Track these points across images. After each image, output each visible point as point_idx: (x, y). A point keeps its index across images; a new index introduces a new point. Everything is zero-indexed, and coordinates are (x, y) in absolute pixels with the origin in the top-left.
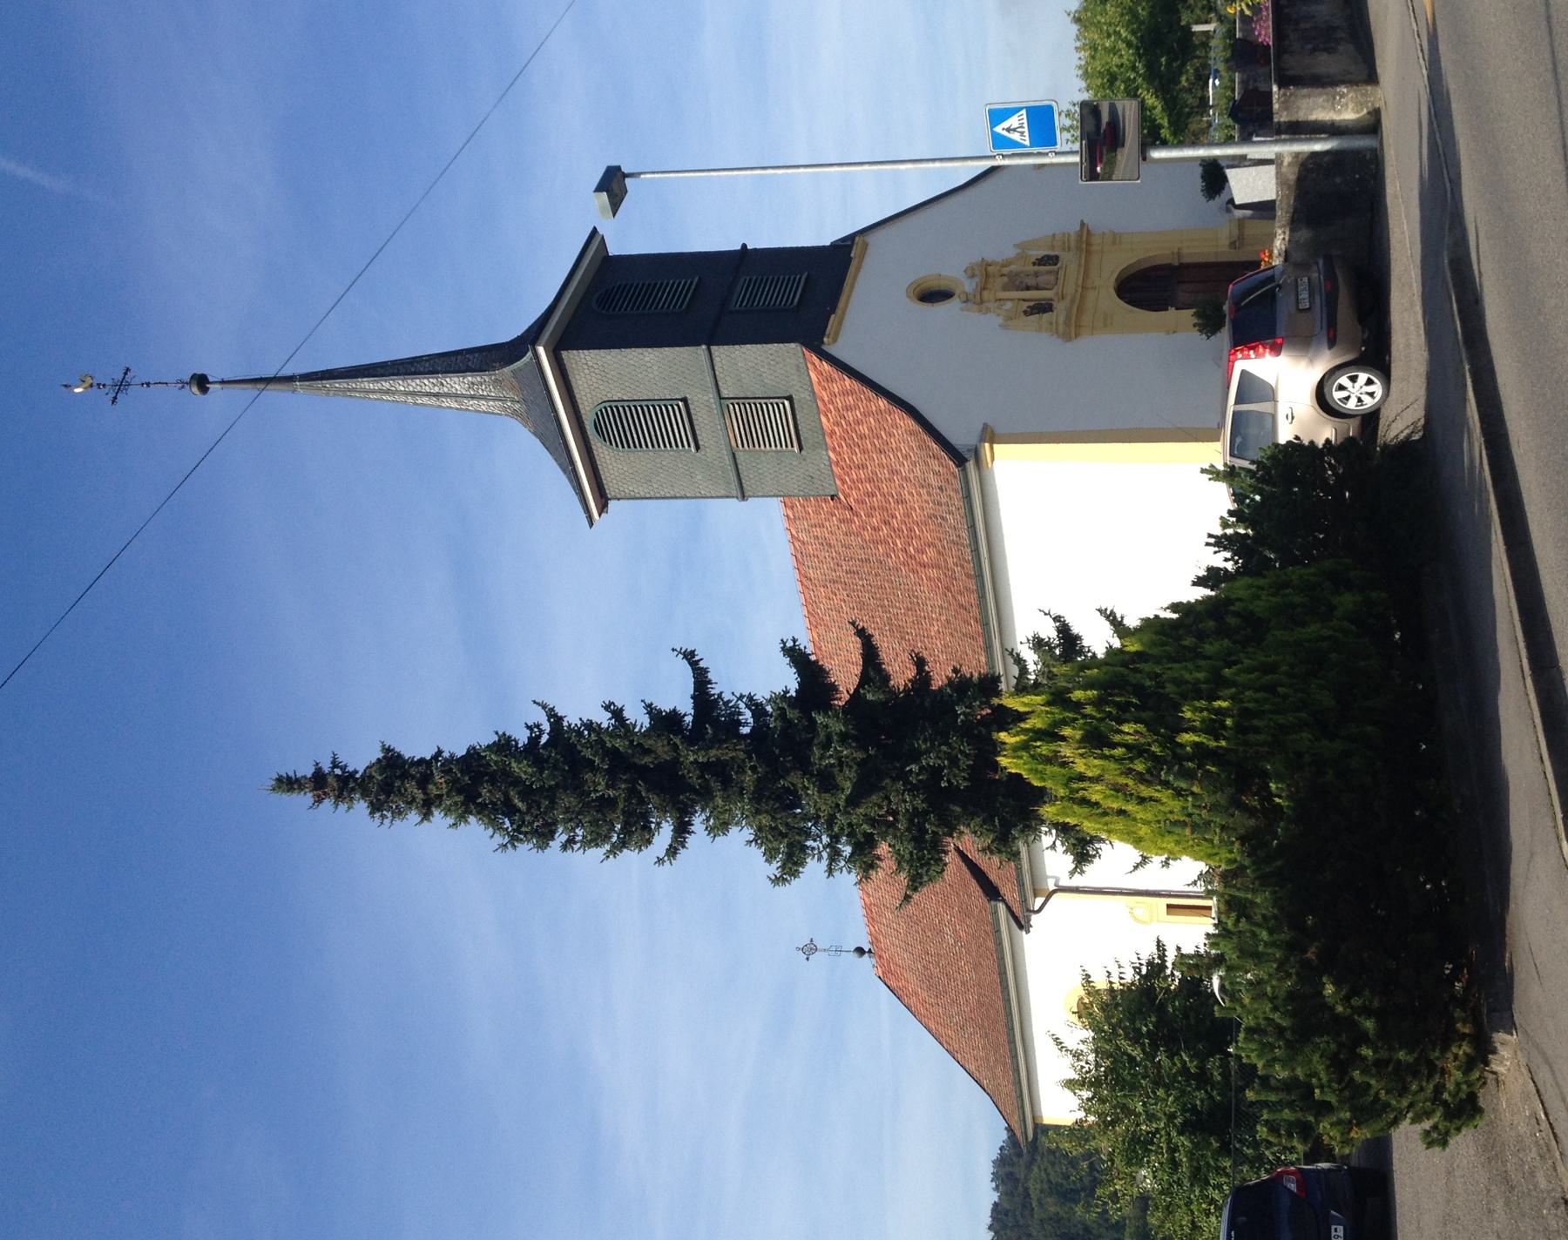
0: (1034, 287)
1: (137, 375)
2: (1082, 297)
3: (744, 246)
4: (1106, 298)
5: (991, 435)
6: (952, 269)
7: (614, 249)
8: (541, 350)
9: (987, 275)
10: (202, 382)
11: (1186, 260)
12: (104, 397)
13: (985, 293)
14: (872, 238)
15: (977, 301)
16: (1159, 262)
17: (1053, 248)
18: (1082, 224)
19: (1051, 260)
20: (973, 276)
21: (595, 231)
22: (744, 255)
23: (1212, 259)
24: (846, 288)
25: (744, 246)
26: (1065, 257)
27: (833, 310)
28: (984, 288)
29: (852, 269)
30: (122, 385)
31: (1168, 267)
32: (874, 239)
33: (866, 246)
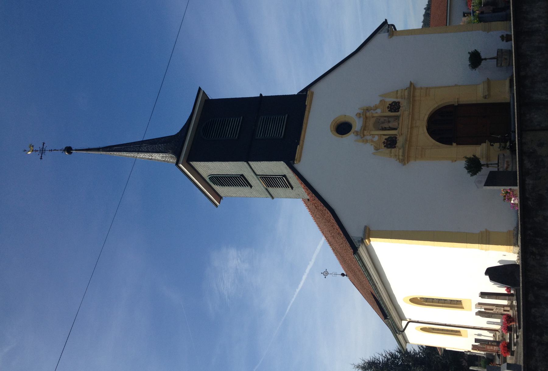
0: (386, 127)
1: (48, 147)
2: (411, 134)
3: (261, 95)
4: (422, 135)
5: (368, 233)
6: (350, 112)
7: (212, 96)
8: (181, 165)
9: (366, 118)
10: (69, 150)
11: (461, 103)
12: (37, 155)
13: (365, 132)
14: (315, 89)
15: (362, 134)
16: (446, 104)
17: (397, 98)
18: (411, 83)
19: (395, 107)
20: (360, 117)
21: (200, 89)
22: (261, 98)
23: (474, 102)
24: (305, 121)
25: (261, 95)
26: (404, 104)
27: (298, 143)
28: (364, 130)
29: (307, 109)
30: (43, 151)
31: (452, 106)
32: (316, 89)
33: (312, 93)
